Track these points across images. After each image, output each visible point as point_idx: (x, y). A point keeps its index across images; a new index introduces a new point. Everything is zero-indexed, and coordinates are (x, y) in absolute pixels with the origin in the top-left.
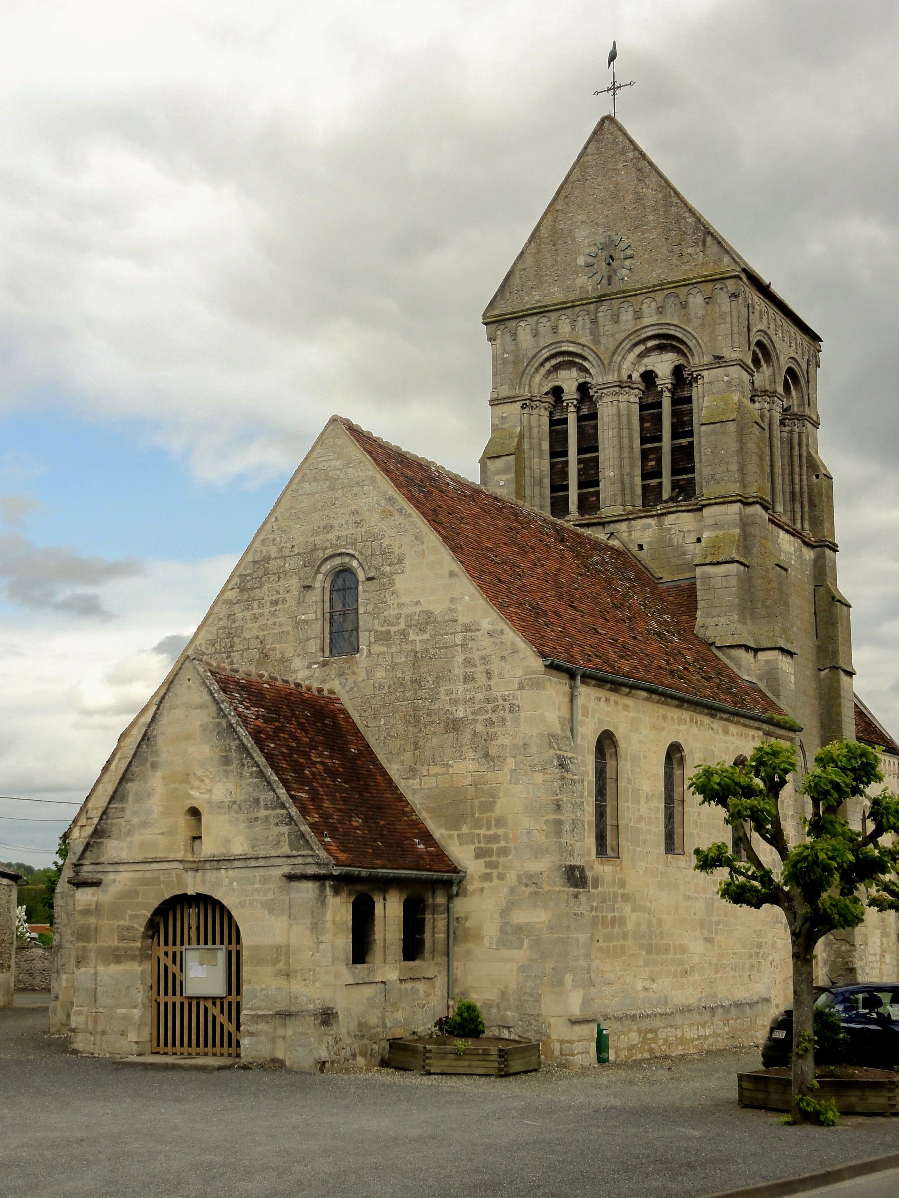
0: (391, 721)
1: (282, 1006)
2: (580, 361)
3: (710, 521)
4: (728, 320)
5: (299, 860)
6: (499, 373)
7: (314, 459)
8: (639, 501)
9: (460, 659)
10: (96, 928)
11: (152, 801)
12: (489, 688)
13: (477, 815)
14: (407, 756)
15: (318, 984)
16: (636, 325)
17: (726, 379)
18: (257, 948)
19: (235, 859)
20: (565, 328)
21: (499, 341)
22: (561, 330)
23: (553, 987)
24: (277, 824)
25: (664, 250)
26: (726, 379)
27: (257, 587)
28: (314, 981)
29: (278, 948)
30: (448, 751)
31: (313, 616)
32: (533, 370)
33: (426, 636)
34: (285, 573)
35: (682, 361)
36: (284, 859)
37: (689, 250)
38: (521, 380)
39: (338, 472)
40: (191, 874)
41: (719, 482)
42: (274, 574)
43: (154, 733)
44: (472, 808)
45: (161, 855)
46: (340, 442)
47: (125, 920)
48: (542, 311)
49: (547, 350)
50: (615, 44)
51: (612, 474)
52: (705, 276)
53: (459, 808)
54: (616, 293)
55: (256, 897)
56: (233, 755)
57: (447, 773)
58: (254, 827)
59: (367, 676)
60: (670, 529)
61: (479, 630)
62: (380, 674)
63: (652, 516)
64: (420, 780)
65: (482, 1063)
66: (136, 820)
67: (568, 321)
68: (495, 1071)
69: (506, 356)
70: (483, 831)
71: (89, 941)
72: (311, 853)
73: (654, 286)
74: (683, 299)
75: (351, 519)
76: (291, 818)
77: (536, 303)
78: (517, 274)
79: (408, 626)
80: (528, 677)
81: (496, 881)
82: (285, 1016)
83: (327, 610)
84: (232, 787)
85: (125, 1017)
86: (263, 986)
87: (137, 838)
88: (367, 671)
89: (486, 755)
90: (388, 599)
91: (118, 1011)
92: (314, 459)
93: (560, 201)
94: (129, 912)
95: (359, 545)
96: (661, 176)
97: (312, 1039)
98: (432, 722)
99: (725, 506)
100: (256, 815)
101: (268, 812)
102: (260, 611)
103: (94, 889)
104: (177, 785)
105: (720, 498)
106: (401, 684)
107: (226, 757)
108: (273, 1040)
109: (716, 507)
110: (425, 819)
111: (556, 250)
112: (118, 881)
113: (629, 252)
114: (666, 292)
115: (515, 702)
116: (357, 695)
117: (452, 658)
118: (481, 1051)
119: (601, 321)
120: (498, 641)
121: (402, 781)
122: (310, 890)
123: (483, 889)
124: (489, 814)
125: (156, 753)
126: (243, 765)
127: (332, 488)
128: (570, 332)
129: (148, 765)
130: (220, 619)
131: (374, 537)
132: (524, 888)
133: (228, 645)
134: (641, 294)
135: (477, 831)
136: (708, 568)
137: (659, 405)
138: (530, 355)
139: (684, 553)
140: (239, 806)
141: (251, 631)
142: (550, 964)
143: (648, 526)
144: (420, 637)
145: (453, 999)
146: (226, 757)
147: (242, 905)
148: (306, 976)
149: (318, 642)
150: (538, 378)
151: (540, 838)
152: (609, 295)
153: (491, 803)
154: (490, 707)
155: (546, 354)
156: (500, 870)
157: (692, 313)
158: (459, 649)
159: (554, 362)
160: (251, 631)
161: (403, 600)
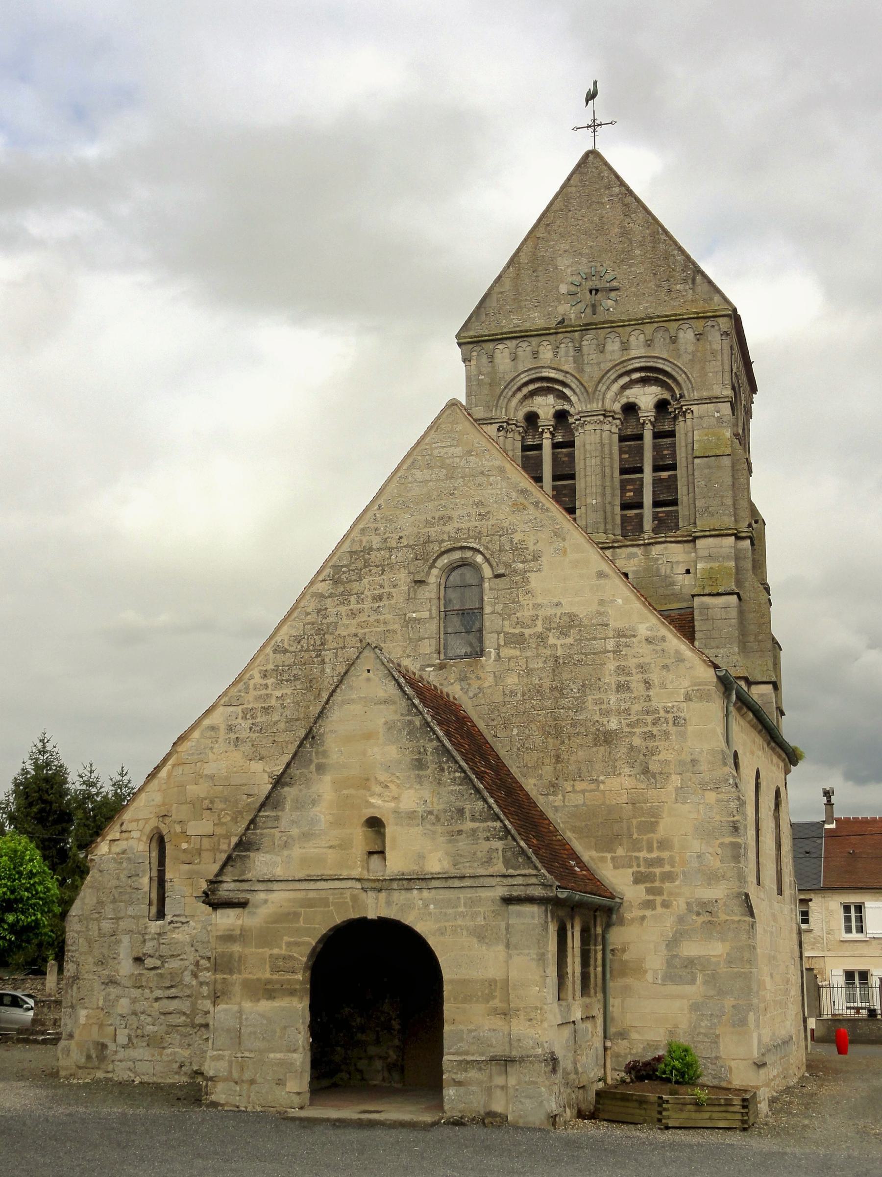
0: (527, 731)
1: (499, 1050)
2: (560, 388)
3: (702, 553)
4: (719, 357)
5: (520, 881)
6: (473, 393)
7: (427, 444)
8: (619, 532)
9: (611, 666)
10: (240, 957)
11: (318, 809)
12: (649, 699)
13: (635, 836)
14: (547, 771)
15: (546, 1025)
16: (622, 355)
17: (716, 415)
18: (464, 982)
19: (432, 878)
20: (546, 354)
21: (473, 362)
22: (541, 356)
23: (734, 1026)
24: (488, 839)
25: (652, 285)
26: (716, 415)
27: (355, 580)
28: (542, 1021)
29: (492, 983)
30: (598, 766)
31: (426, 614)
32: (510, 393)
33: (569, 640)
34: (391, 566)
35: (667, 396)
36: (498, 879)
37: (678, 287)
38: (498, 402)
39: (457, 460)
40: (371, 894)
41: (713, 515)
42: (377, 566)
43: (321, 731)
44: (629, 829)
45: (329, 872)
46: (459, 428)
47: (281, 948)
48: (523, 336)
49: (526, 374)
50: (595, 83)
51: (594, 502)
52: (697, 313)
53: (610, 830)
54: (603, 323)
55: (460, 922)
56: (430, 758)
57: (597, 789)
58: (457, 841)
59: (496, 681)
60: (657, 559)
61: (634, 636)
62: (512, 680)
63: (638, 545)
64: (564, 796)
65: (724, 1114)
66: (295, 831)
67: (549, 347)
68: (737, 1124)
69: (481, 377)
70: (643, 854)
71: (231, 972)
72: (534, 872)
73: (643, 319)
74: (673, 334)
75: (474, 511)
76: (508, 832)
77: (514, 327)
78: (494, 297)
79: (547, 629)
80: (696, 688)
81: (659, 910)
82: (505, 1062)
83: (442, 609)
84: (426, 794)
85: (281, 1063)
86: (472, 1027)
87: (296, 852)
88: (495, 676)
89: (646, 771)
90: (521, 599)
91: (272, 1055)
92: (427, 444)
93: (541, 229)
94: (286, 939)
95: (485, 540)
96: (649, 213)
97: (543, 1089)
98: (578, 734)
99: (720, 539)
100: (460, 827)
101: (475, 825)
102: (359, 606)
103: (238, 911)
104: (351, 791)
105: (714, 530)
106: (538, 692)
107: (419, 760)
108: (489, 1091)
109: (711, 540)
110: (571, 841)
111: (537, 276)
112: (270, 903)
113: (615, 284)
114: (656, 325)
115: (680, 714)
116: (483, 702)
117: (601, 665)
118: (722, 1101)
119: (585, 350)
120: (659, 648)
121: (540, 797)
122: (536, 915)
123: (643, 918)
124: (651, 835)
125: (325, 754)
126: (442, 770)
127: (450, 477)
128: (550, 357)
129: (313, 767)
130: (308, 614)
131: (503, 532)
132: (694, 917)
133: (318, 643)
134: (629, 325)
135: (635, 854)
136: (706, 599)
137: (640, 437)
138: (508, 378)
139: (672, 584)
140: (437, 817)
141: (348, 627)
142: (729, 1002)
143: (634, 555)
144: (563, 641)
145: (610, 1039)
146: (419, 760)
147: (442, 932)
148: (532, 1015)
149: (434, 642)
150: (515, 402)
151: (715, 863)
152: (596, 324)
153: (652, 823)
154: (649, 719)
155: (525, 378)
156: (665, 897)
157: (682, 348)
158: (611, 655)
159: (532, 387)
160: (348, 627)
161: (539, 600)
